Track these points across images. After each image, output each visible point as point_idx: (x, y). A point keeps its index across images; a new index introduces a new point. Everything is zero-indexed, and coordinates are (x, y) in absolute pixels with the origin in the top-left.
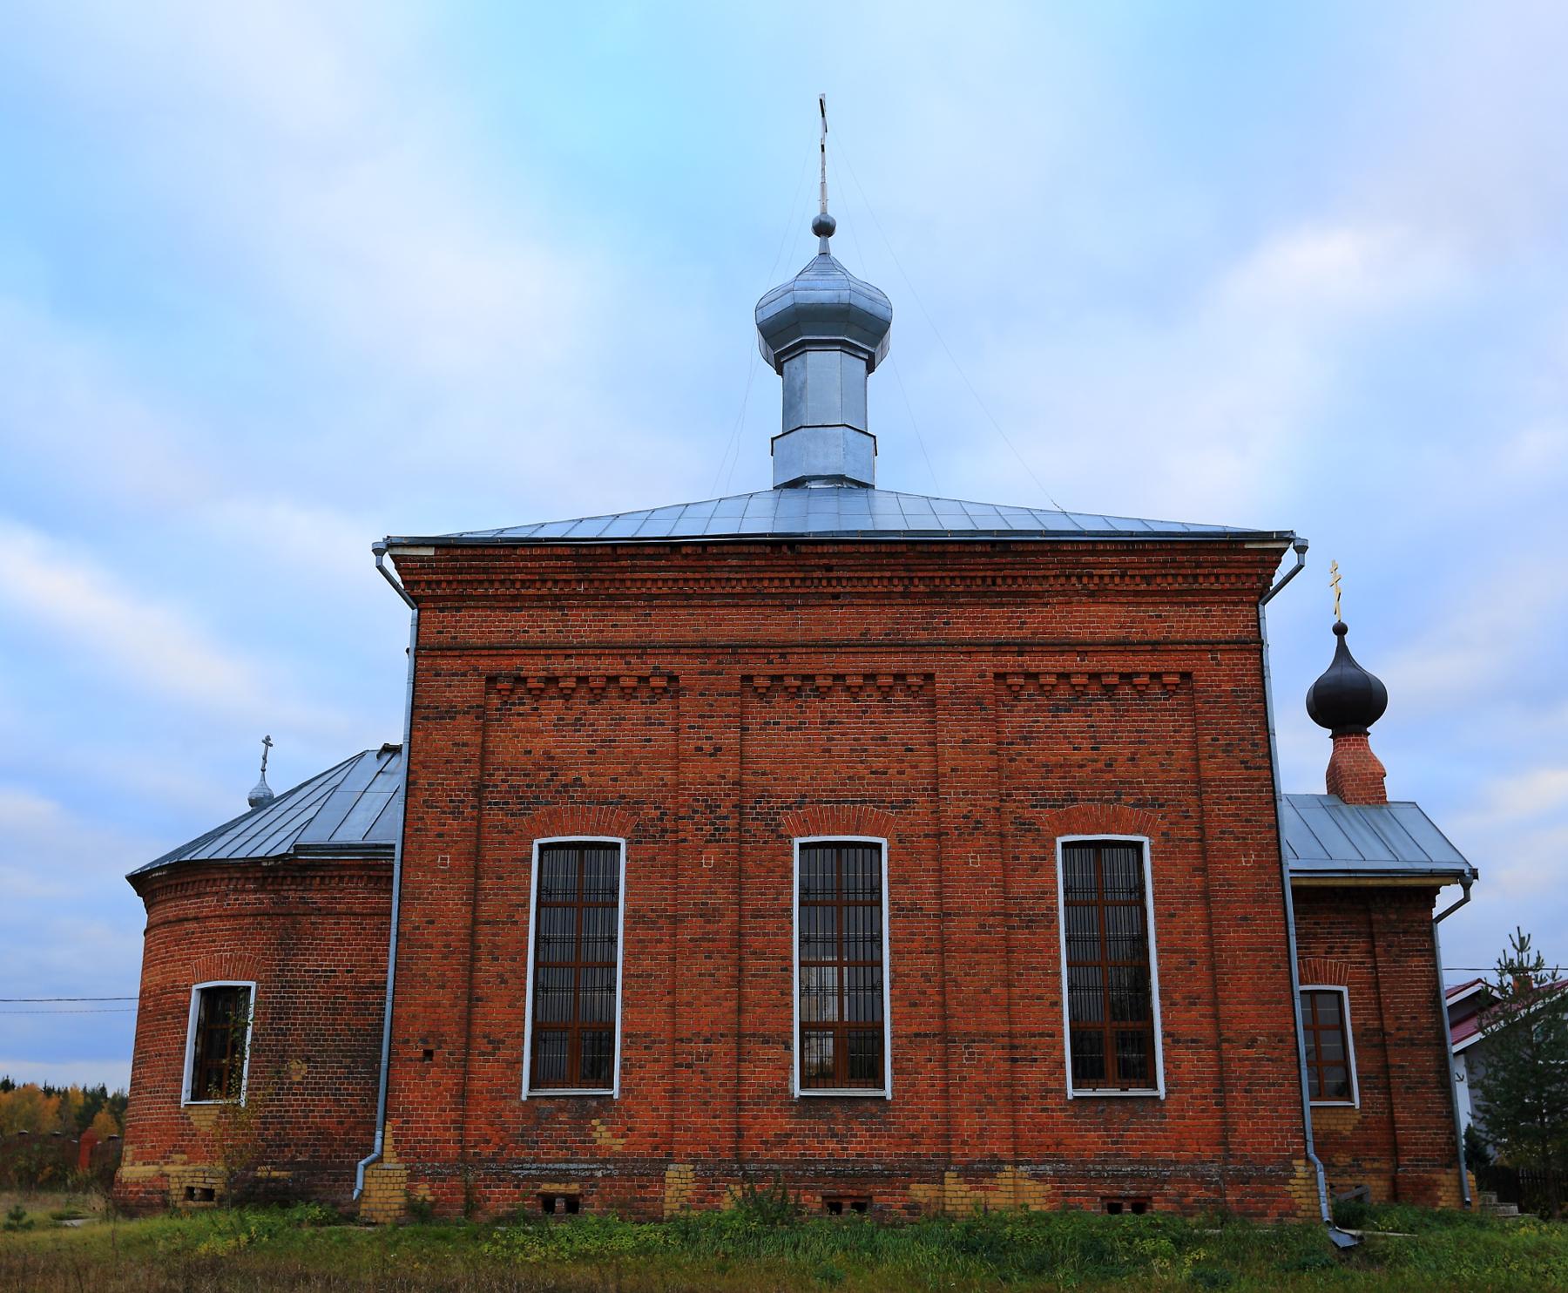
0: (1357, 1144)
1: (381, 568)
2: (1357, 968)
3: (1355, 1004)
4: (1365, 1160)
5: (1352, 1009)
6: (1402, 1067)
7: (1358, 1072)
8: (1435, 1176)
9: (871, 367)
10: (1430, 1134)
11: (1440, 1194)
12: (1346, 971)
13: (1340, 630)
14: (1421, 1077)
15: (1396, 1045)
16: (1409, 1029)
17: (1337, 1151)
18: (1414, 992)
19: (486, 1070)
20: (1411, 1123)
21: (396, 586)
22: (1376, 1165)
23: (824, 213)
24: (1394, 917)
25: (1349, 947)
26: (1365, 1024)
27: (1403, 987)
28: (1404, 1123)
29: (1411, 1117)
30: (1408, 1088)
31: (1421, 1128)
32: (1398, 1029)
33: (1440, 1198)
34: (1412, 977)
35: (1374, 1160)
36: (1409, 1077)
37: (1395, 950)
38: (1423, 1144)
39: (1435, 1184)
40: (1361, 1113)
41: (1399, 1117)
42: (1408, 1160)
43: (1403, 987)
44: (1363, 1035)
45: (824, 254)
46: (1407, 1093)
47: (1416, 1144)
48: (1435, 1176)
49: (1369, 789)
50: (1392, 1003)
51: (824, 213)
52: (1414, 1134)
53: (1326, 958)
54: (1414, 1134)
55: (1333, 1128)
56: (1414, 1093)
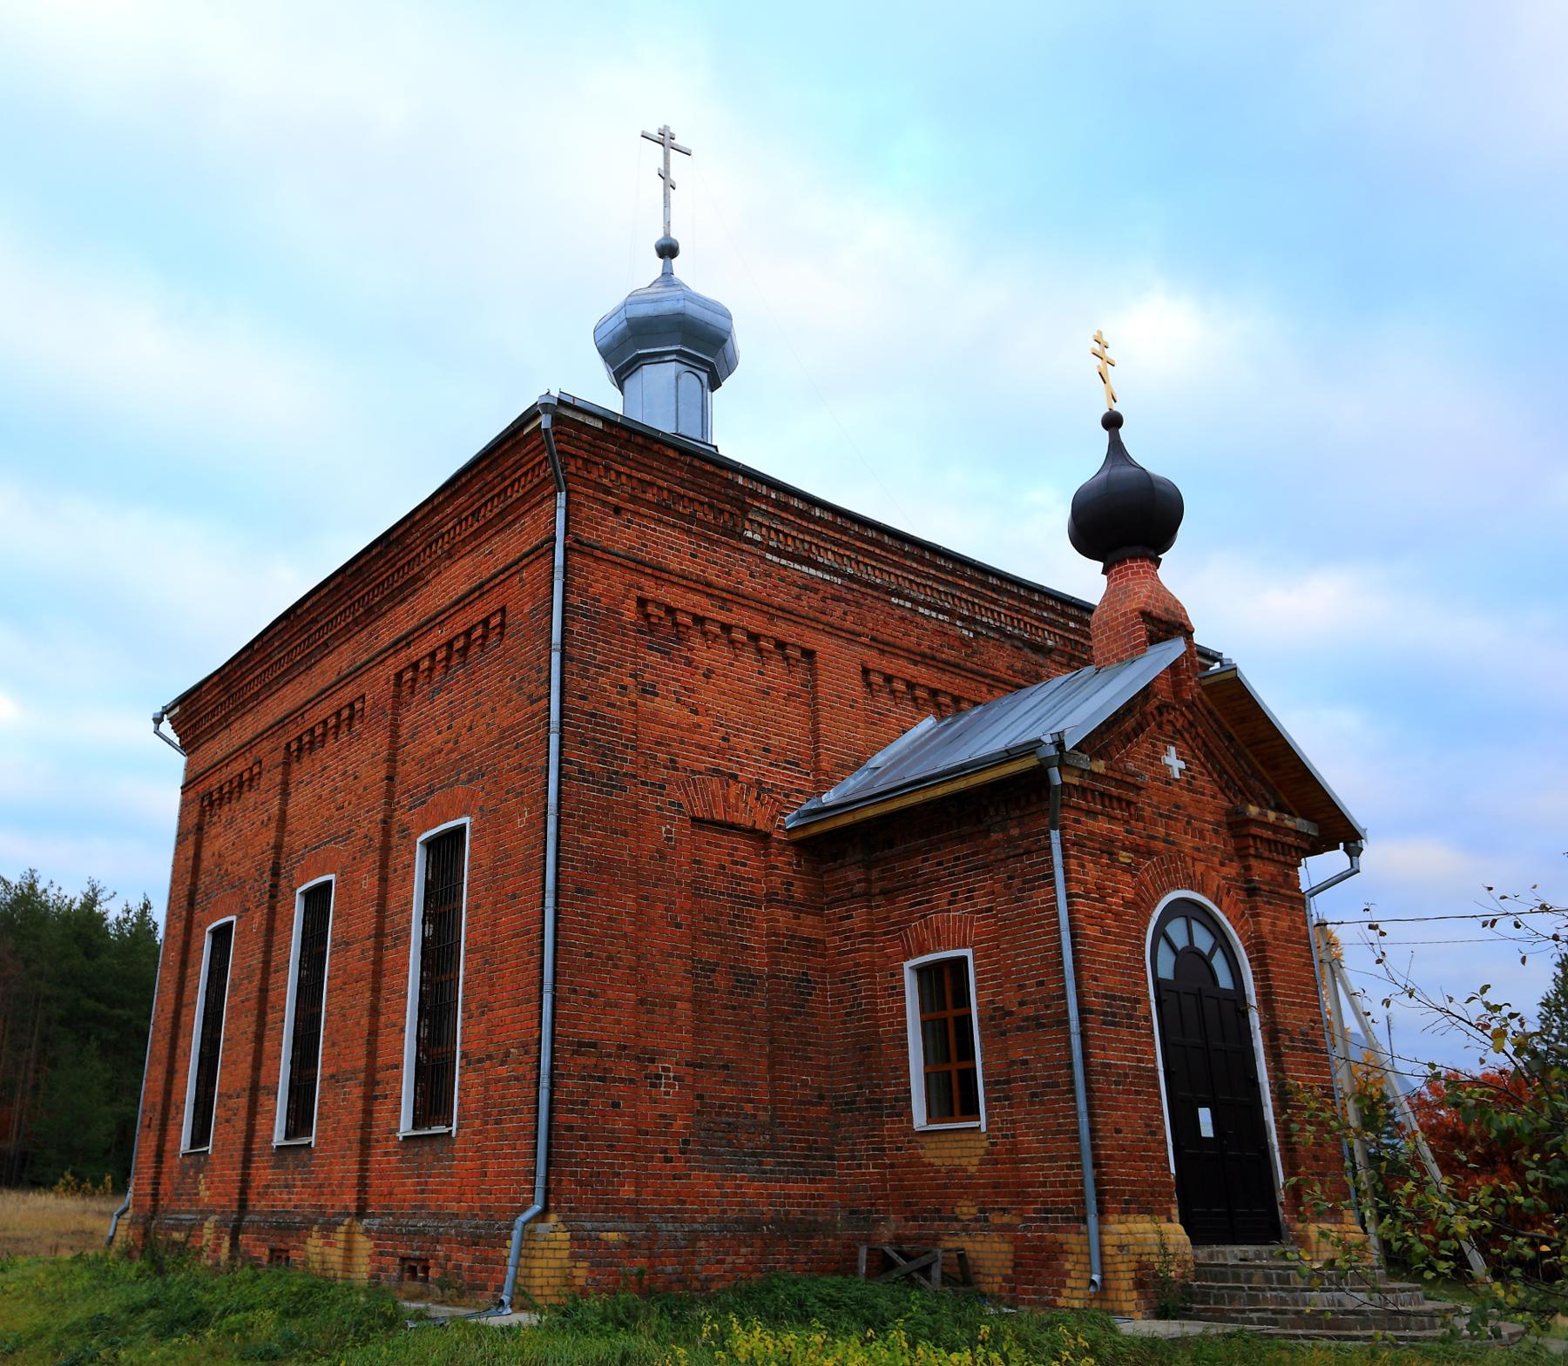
0: (984, 1186)
1: (157, 732)
2: (984, 919)
3: (984, 973)
4: (993, 1209)
5: (978, 981)
6: (1025, 1062)
7: (984, 1076)
8: (1061, 1237)
9: (715, 384)
10: (1061, 1168)
11: (1068, 1266)
12: (972, 926)
13: (1112, 422)
14: (1050, 1077)
15: (1019, 1028)
16: (1034, 1002)
17: (960, 1196)
18: (1040, 943)
19: (382, 1111)
20: (1037, 1150)
21: (170, 743)
22: (1006, 1219)
23: (667, 235)
24: (1015, 832)
25: (973, 890)
26: (992, 1002)
27: (1028, 937)
28: (1028, 1151)
29: (1038, 1141)
30: (1034, 1095)
31: (1051, 1159)
32: (1021, 1004)
33: (1067, 1274)
34: (1040, 919)
35: (1004, 1210)
36: (1034, 1078)
37: (1016, 882)
38: (1053, 1184)
39: (1059, 1251)
40: (989, 1137)
41: (1022, 1142)
42: (1036, 1210)
43: (1028, 937)
44: (992, 1018)
45: (667, 274)
46: (1032, 1103)
47: (1043, 1184)
48: (1061, 1237)
49: (1122, 638)
50: (1015, 964)
51: (667, 235)
52: (1042, 1169)
53: (949, 911)
54: (1042, 1169)
55: (957, 1162)
56: (1042, 1103)
